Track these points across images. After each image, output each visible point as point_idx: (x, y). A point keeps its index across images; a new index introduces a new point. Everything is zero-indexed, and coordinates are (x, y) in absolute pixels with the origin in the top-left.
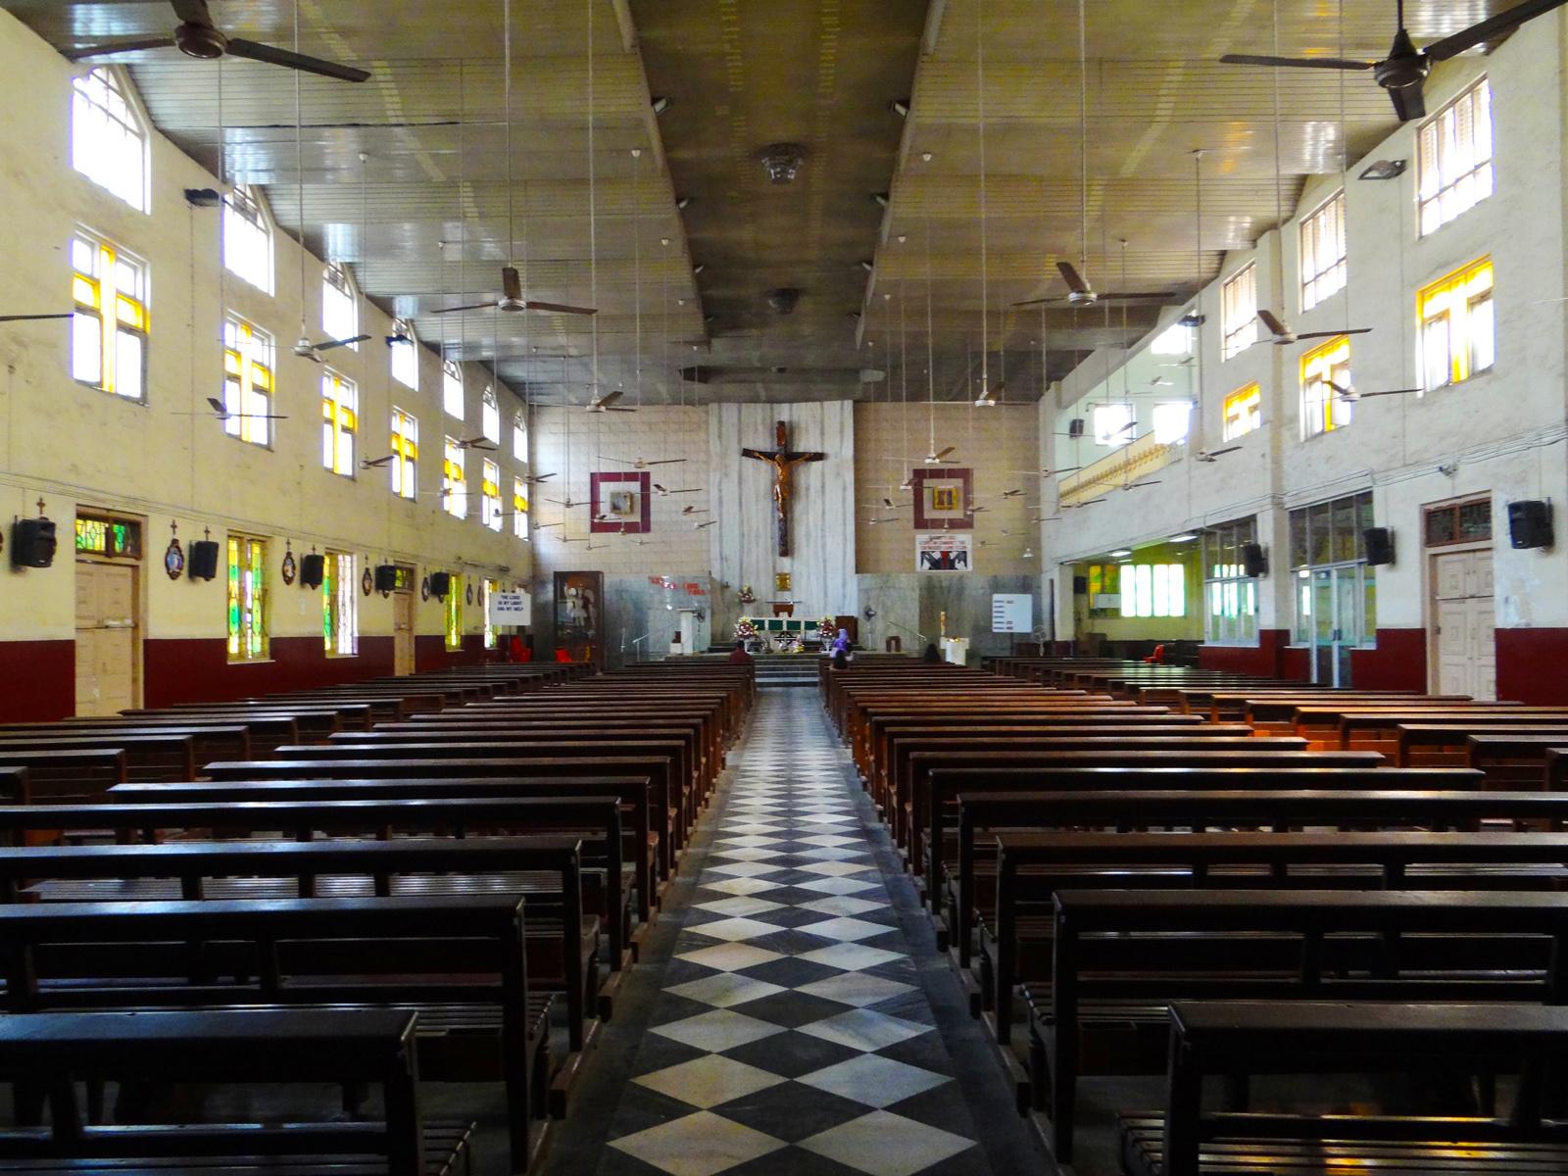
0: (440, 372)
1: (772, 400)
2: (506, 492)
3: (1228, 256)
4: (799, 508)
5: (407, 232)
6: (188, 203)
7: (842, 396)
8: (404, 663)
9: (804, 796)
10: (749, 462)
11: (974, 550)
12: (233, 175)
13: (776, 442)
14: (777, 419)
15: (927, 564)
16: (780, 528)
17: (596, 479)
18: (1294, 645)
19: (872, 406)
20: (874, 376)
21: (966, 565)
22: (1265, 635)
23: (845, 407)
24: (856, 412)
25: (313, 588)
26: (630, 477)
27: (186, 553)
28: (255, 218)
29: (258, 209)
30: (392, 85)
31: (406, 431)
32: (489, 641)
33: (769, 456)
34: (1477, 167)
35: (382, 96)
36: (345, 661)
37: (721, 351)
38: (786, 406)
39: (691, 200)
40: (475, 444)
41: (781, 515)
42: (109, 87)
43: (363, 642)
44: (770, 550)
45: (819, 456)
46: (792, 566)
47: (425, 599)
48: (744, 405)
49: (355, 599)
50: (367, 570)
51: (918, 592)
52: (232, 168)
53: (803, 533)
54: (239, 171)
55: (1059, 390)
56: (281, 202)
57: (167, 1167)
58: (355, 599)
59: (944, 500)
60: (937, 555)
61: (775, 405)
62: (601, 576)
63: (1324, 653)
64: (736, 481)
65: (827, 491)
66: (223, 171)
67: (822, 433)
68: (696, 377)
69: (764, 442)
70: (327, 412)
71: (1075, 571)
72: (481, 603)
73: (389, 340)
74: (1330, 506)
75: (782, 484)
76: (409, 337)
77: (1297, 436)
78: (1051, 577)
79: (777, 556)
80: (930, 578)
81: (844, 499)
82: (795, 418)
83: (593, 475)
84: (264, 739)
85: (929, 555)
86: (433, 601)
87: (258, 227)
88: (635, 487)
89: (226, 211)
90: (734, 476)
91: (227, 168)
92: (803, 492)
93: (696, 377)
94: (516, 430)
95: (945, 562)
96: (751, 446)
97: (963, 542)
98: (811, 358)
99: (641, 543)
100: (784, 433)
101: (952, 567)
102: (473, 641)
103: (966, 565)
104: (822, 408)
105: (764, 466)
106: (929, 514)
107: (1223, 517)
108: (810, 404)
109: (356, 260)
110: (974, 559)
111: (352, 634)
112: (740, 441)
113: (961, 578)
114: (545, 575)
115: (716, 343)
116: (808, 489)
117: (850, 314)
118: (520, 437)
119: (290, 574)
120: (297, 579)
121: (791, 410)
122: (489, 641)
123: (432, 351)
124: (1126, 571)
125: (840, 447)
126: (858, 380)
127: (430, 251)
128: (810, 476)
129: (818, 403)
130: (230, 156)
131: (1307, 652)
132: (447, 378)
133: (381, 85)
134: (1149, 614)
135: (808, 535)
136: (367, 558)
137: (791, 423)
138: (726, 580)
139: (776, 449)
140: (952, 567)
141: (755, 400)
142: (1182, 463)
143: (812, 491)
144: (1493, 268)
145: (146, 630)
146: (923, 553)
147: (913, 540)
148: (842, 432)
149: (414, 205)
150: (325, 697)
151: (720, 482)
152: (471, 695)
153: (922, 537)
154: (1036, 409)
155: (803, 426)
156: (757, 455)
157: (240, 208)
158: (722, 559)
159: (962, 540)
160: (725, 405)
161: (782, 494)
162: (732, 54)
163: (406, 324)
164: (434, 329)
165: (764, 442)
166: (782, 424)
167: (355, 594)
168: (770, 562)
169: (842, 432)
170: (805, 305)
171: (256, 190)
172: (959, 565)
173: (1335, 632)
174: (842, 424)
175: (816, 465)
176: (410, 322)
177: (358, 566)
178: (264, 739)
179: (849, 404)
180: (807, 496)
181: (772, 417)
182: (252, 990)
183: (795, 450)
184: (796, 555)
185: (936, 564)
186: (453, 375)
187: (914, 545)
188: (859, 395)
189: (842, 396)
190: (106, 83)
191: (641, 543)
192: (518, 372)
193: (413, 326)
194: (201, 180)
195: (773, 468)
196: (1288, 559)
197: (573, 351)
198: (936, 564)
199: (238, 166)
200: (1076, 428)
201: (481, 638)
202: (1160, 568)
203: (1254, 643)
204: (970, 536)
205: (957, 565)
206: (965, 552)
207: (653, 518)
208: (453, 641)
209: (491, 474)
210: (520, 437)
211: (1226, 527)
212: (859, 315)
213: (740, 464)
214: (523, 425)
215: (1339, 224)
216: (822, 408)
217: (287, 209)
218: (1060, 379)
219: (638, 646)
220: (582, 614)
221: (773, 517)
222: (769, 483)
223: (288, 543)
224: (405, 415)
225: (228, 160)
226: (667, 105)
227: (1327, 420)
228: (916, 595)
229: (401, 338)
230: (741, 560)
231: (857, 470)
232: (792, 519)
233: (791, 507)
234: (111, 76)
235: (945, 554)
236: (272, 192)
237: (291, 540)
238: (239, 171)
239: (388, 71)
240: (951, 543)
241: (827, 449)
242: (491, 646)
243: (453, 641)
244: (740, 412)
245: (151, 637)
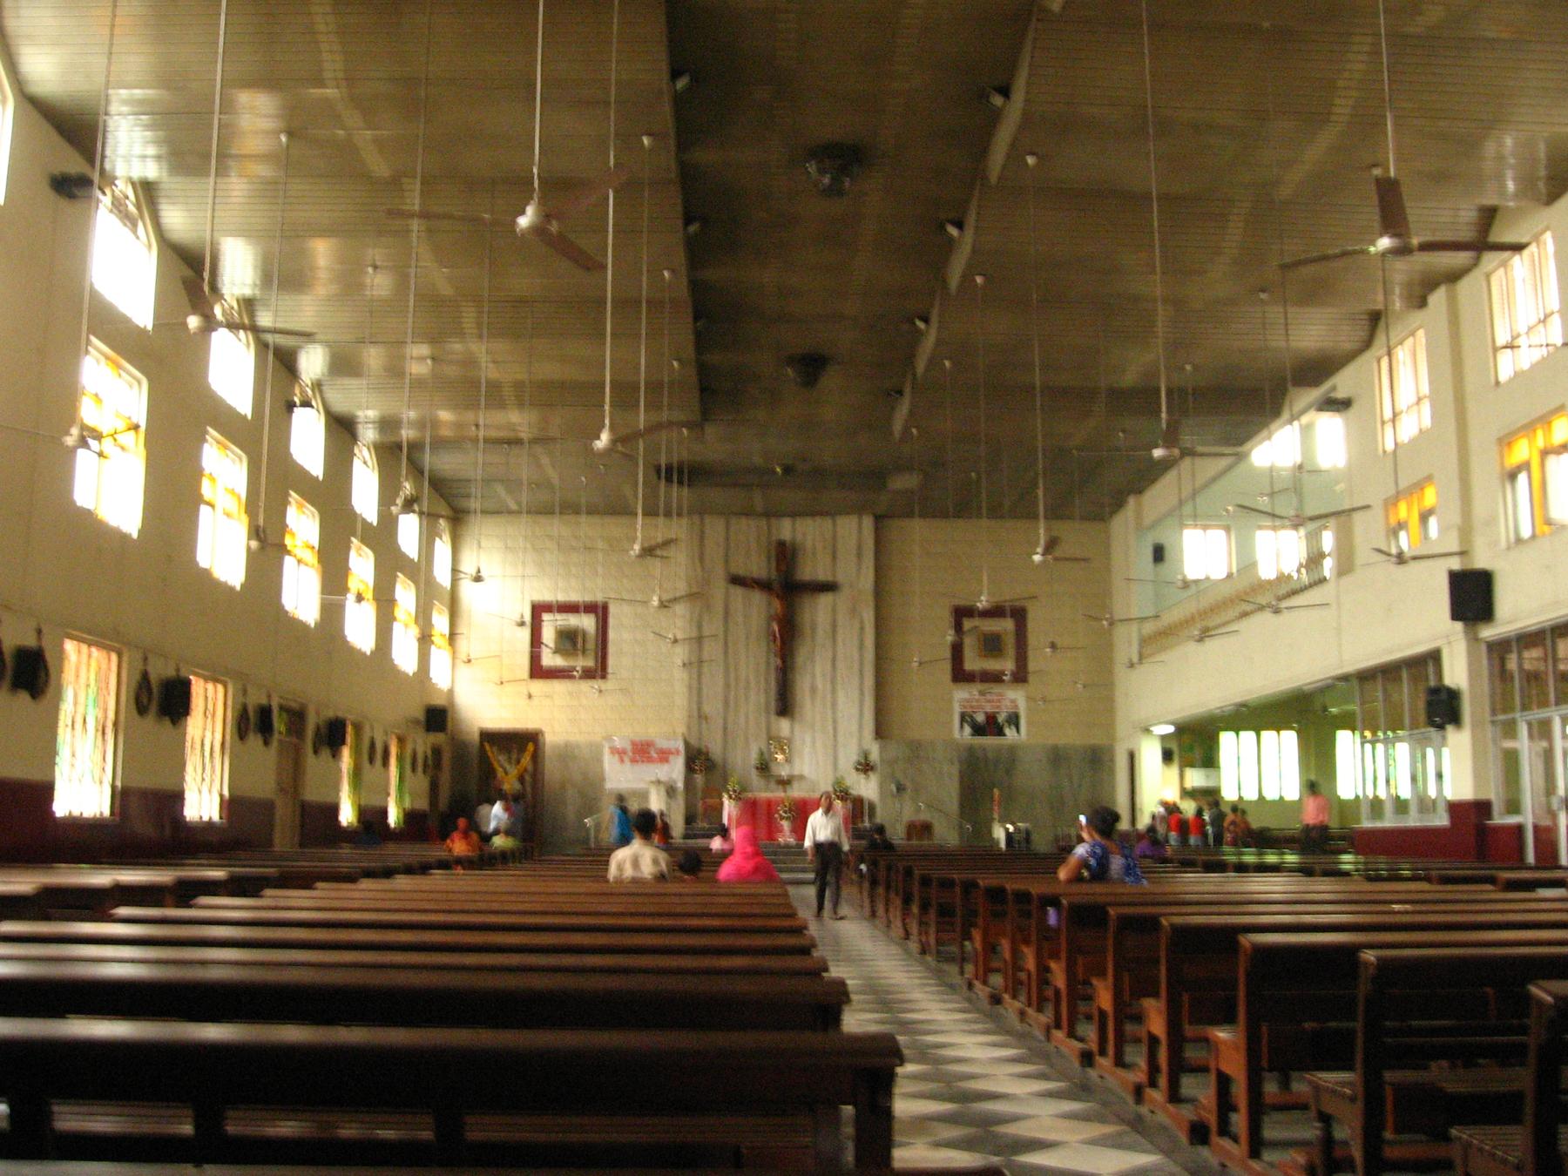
0: (351, 455)
1: (771, 514)
2: (423, 617)
3: (1499, 216)
5: (322, 252)
7: (859, 510)
10: (738, 592)
13: (774, 565)
15: (968, 730)
17: (538, 610)
19: (896, 524)
20: (904, 482)
22: (1455, 808)
31: (303, 525)
32: (393, 817)
33: (763, 585)
40: (390, 563)
43: (231, 805)
45: (829, 587)
48: (733, 521)
49: (228, 745)
57: (1543, 293)
58: (228, 745)
59: (992, 645)
61: (773, 521)
67: (834, 558)
69: (758, 565)
74: (1514, 644)
76: (314, 403)
77: (1496, 543)
82: (799, 537)
85: (971, 717)
86: (326, 753)
92: (807, 630)
95: (991, 726)
100: (785, 555)
101: (1000, 733)
105: (758, 598)
106: (972, 663)
107: (839, 972)
108: (818, 520)
110: (1029, 724)
115: (711, 431)
116: (814, 629)
118: (442, 548)
119: (145, 701)
122: (393, 817)
123: (342, 428)
124: (1226, 739)
125: (858, 576)
127: (349, 283)
128: (818, 612)
131: (1519, 829)
135: (813, 690)
140: (1000, 733)
141: (748, 513)
148: (859, 555)
153: (962, 695)
158: (700, 717)
159: (1014, 698)
160: (708, 520)
164: (343, 397)
166: (781, 545)
167: (228, 737)
168: (763, 725)
169: (859, 555)
172: (1010, 732)
174: (859, 548)
175: (825, 600)
178: (95, 904)
179: (868, 523)
180: (813, 639)
184: (797, 715)
185: (978, 730)
192: (446, 463)
193: (321, 392)
198: (978, 730)
201: (384, 813)
202: (1268, 736)
205: (1007, 731)
209: (405, 594)
210: (442, 548)
211: (1388, 673)
214: (447, 538)
218: (1140, 492)
227: (1538, 521)
228: (955, 770)
244: (728, 528)
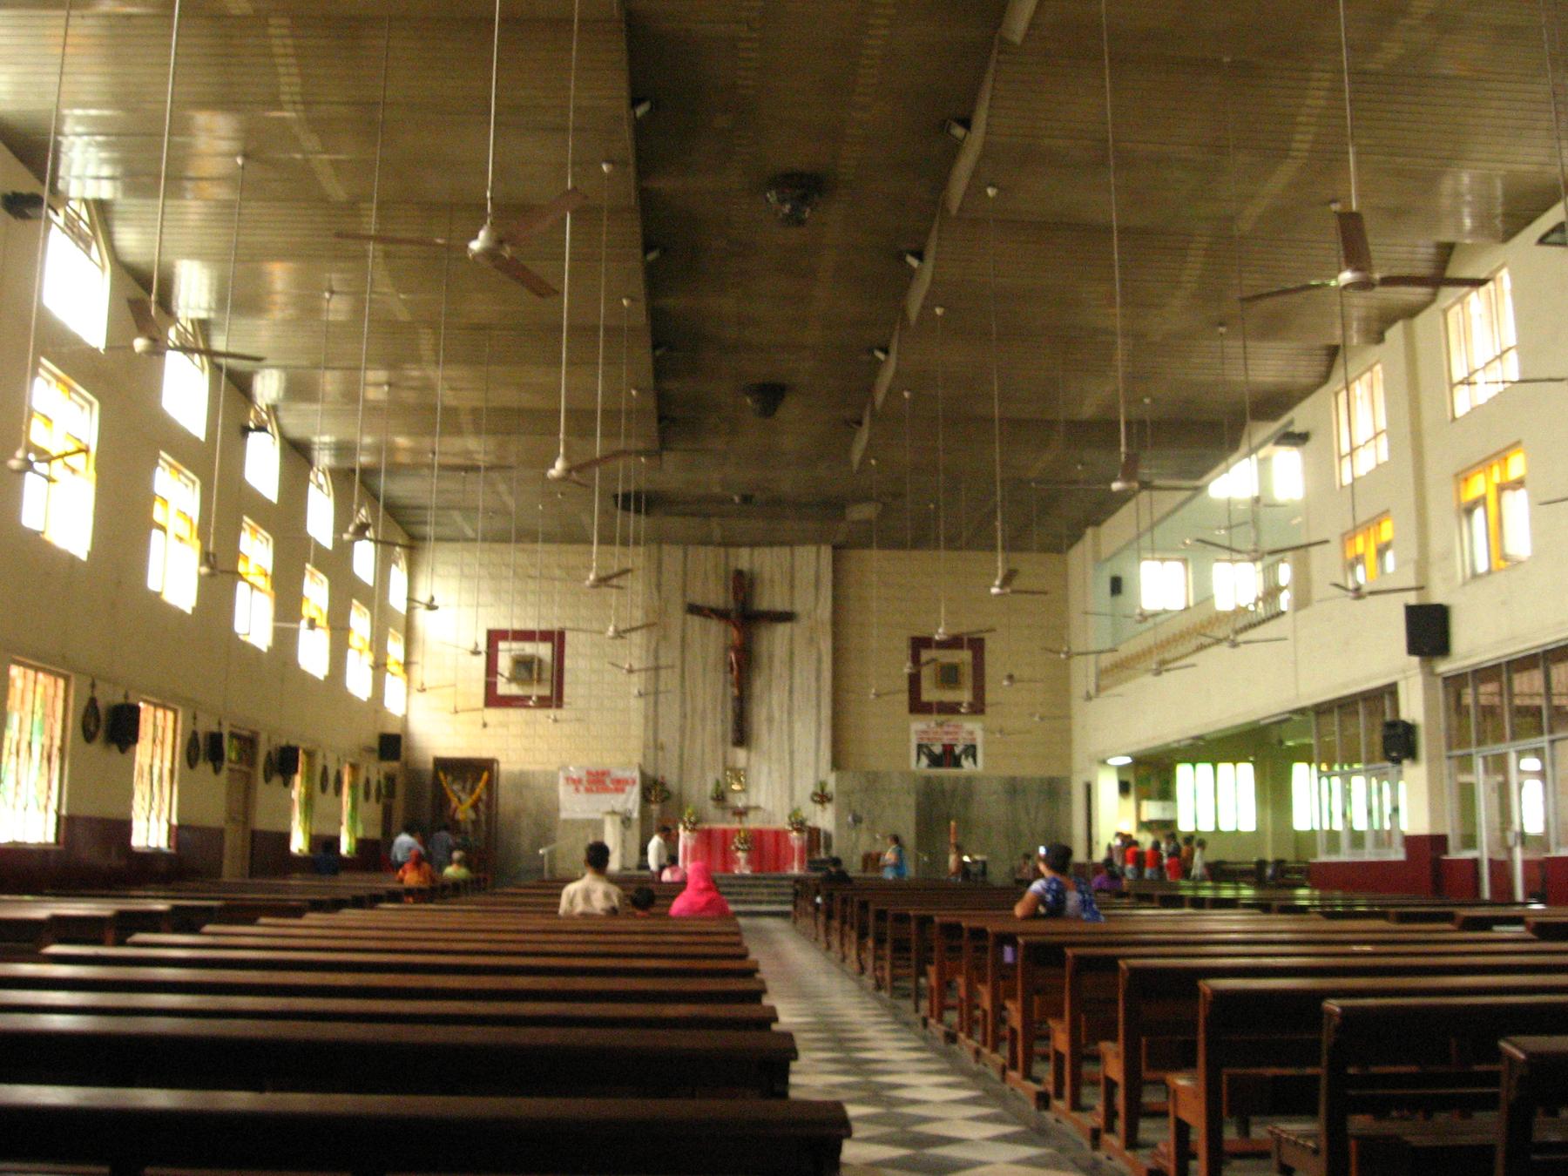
1: (729, 543)
2: (378, 644)
4: (758, 685)
9: (822, 1040)
10: (696, 621)
11: (986, 743)
12: (68, 185)
14: (733, 564)
15: (924, 761)
17: (494, 637)
18: (1456, 853)
19: (854, 554)
21: (975, 761)
22: (1412, 842)
26: (546, 636)
28: (88, 247)
32: (346, 846)
34: (1504, 352)
35: (275, 65)
36: (150, 858)
37: (672, 474)
38: (744, 553)
39: (665, 251)
41: (736, 691)
43: (178, 833)
45: (787, 617)
46: (749, 759)
47: (267, 780)
48: (690, 548)
50: (195, 734)
51: (914, 796)
52: (69, 173)
55: (1096, 537)
60: (937, 749)
61: (732, 551)
62: (495, 765)
63: (1501, 870)
65: (797, 659)
68: (632, 507)
69: (717, 595)
72: (338, 791)
79: (729, 744)
82: (757, 568)
86: (277, 780)
87: (91, 259)
88: (544, 650)
90: (676, 636)
91: (62, 172)
93: (632, 507)
95: (948, 757)
97: (971, 733)
98: (788, 482)
99: (556, 720)
100: (743, 584)
102: (325, 845)
104: (792, 555)
105: (715, 626)
108: (776, 549)
110: (986, 755)
111: (169, 821)
112: (684, 594)
115: (668, 457)
117: (847, 423)
118: (398, 574)
119: (92, 728)
120: (101, 735)
121: (751, 555)
122: (346, 846)
123: (297, 453)
124: (1183, 771)
125: (816, 606)
126: (843, 518)
127: (307, 306)
128: (776, 640)
129: (787, 550)
130: (66, 154)
131: (1475, 863)
132: (312, 488)
135: (770, 720)
136: (195, 718)
138: (660, 773)
140: (957, 763)
141: (705, 542)
142: (1283, 619)
146: (920, 747)
147: (907, 730)
150: (126, 897)
153: (919, 726)
154: (1065, 564)
155: (767, 576)
156: (707, 612)
157: (71, 226)
159: (971, 729)
160: (666, 548)
162: (750, 40)
165: (717, 595)
166: (739, 574)
168: (720, 753)
170: (789, 410)
171: (92, 207)
172: (967, 764)
173: (1516, 834)
175: (782, 630)
177: (183, 729)
179: (826, 552)
180: (770, 668)
181: (727, 564)
182: (1350, 202)
184: (754, 745)
185: (936, 761)
186: (320, 487)
187: (908, 735)
188: (840, 538)
189: (818, 540)
191: (556, 720)
195: (726, 631)
196: (1443, 742)
197: (481, 459)
198: (936, 761)
199: (75, 171)
200: (1116, 586)
203: (1398, 854)
207: (567, 690)
209: (360, 621)
210: (398, 574)
211: (1344, 706)
213: (684, 623)
214: (403, 564)
215: (1376, 394)
216: (792, 555)
217: (130, 240)
219: (546, 859)
221: (724, 694)
223: (93, 686)
226: (652, 108)
230: (682, 748)
231: (837, 636)
232: (750, 697)
233: (749, 678)
235: (948, 749)
237: (98, 682)
238: (78, 177)
239: (289, 42)
240: (956, 733)
241: (798, 608)
242: (348, 852)
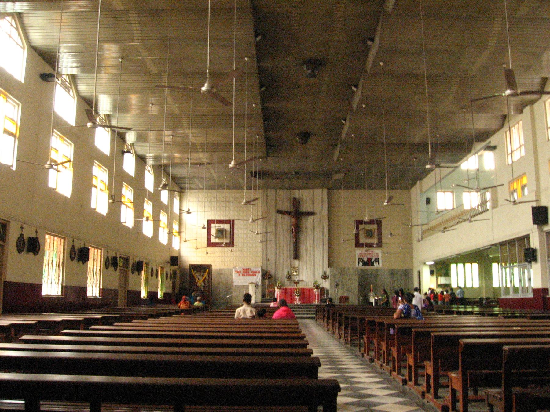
1: (291, 188)
2: (170, 225)
4: (302, 237)
6: (41, 80)
8: (121, 303)
14: (292, 197)
15: (361, 264)
16: (294, 246)
17: (210, 222)
21: (379, 264)
22: (535, 291)
23: (324, 192)
24: (329, 194)
25: (83, 263)
27: (26, 241)
28: (69, 91)
29: (71, 87)
30: (137, 25)
31: (128, 194)
32: (160, 295)
33: (289, 213)
37: (272, 164)
38: (296, 191)
42: (12, 25)
43: (103, 291)
44: (289, 256)
45: (312, 214)
53: (304, 249)
54: (65, 67)
55: (421, 184)
56: (81, 84)
59: (369, 234)
60: (365, 260)
64: (274, 224)
66: (58, 68)
69: (286, 206)
70: (94, 182)
71: (430, 268)
72: (157, 277)
73: (123, 152)
75: (294, 225)
76: (131, 152)
78: (418, 269)
79: (292, 260)
80: (362, 271)
81: (323, 234)
83: (208, 221)
84: (55, 328)
87: (70, 95)
88: (227, 227)
89: (57, 86)
90: (273, 222)
92: (304, 229)
94: (175, 198)
95: (369, 262)
96: (281, 209)
97: (377, 254)
98: (311, 167)
100: (296, 202)
102: (152, 295)
103: (379, 264)
105: (287, 218)
109: (111, 113)
111: (99, 287)
113: (377, 270)
114: (185, 266)
117: (332, 145)
118: (176, 201)
123: (141, 160)
125: (322, 210)
127: (143, 110)
128: (308, 222)
132: (146, 172)
133: (133, 25)
134: (471, 287)
135: (306, 250)
137: (299, 199)
139: (292, 210)
140: (372, 264)
141: (283, 188)
143: (308, 230)
144: (474, 263)
145: (5, 277)
146: (359, 259)
148: (322, 202)
149: (140, 86)
151: (267, 224)
152: (151, 316)
153: (359, 252)
157: (63, 84)
159: (377, 252)
160: (269, 190)
161: (295, 231)
163: (131, 146)
166: (295, 199)
170: (312, 141)
172: (376, 265)
176: (132, 145)
177: (104, 254)
178: (55, 328)
179: (325, 191)
183: (301, 210)
185: (365, 264)
186: (149, 171)
190: (11, 23)
194: (48, 70)
197: (204, 161)
198: (365, 264)
204: (381, 251)
205: (375, 264)
206: (379, 259)
208: (144, 294)
209: (163, 217)
210: (176, 201)
211: (510, 243)
212: (336, 146)
213: (276, 217)
217: (83, 88)
218: (421, 179)
220: (203, 284)
222: (289, 226)
224: (128, 187)
225: (61, 61)
228: (356, 278)
229: (129, 152)
234: (13, 20)
236: (78, 80)
238: (65, 67)
239: (136, 19)
243: (144, 294)
245: (7, 280)
